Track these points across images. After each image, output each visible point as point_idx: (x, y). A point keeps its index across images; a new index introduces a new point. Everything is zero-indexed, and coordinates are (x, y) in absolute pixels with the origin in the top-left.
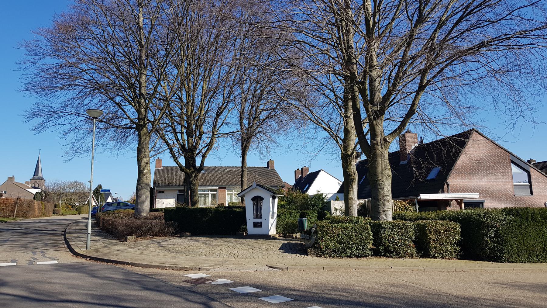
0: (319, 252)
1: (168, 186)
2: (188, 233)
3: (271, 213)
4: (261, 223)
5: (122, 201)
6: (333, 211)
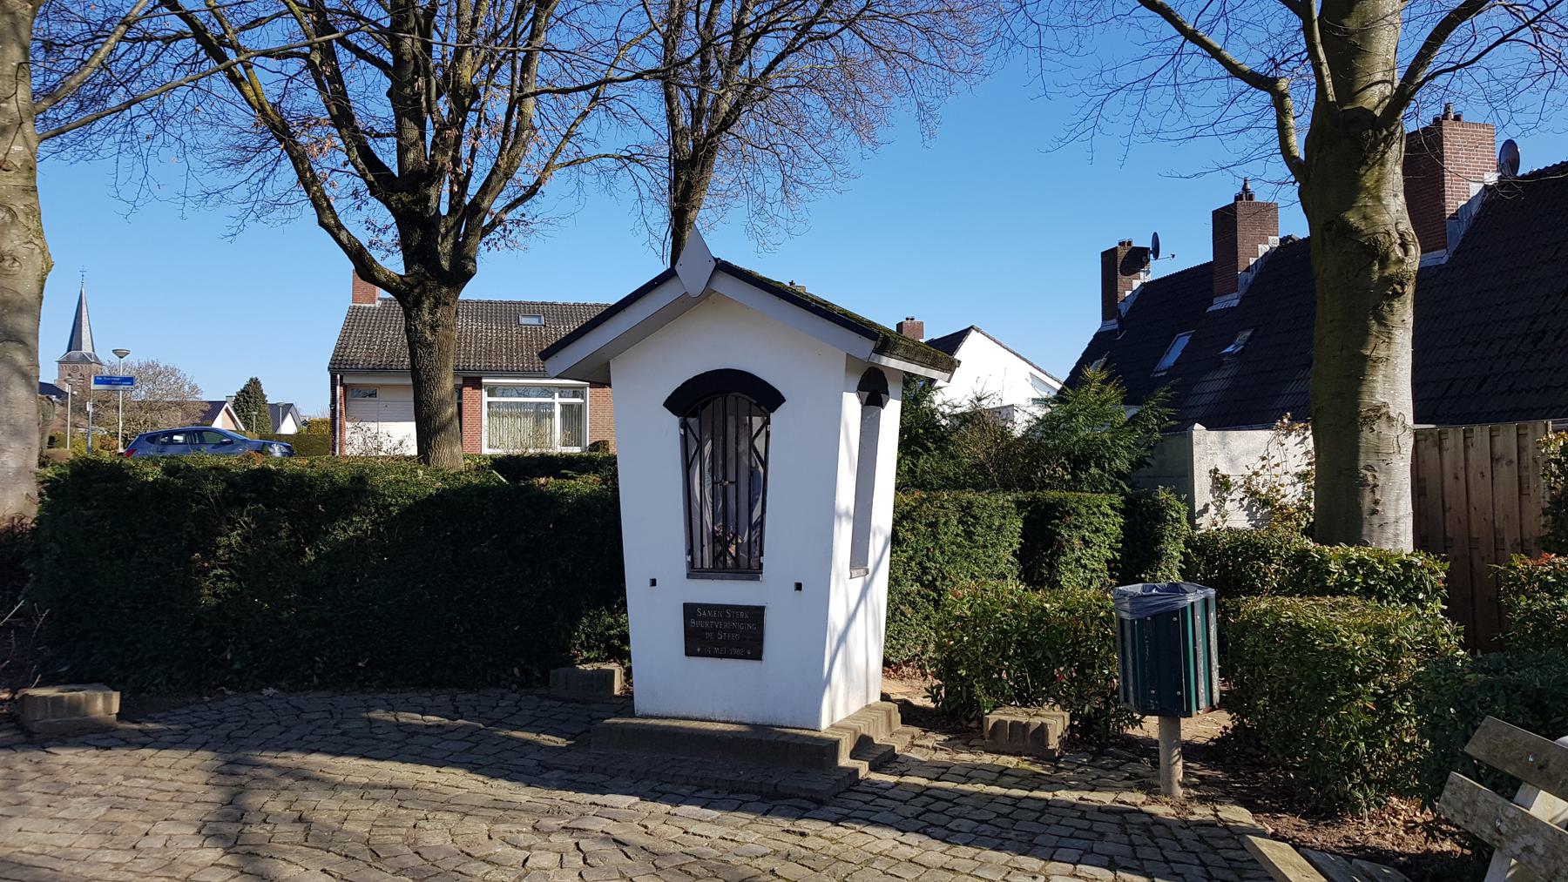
2: (104, 704)
3: (843, 535)
4: (756, 614)
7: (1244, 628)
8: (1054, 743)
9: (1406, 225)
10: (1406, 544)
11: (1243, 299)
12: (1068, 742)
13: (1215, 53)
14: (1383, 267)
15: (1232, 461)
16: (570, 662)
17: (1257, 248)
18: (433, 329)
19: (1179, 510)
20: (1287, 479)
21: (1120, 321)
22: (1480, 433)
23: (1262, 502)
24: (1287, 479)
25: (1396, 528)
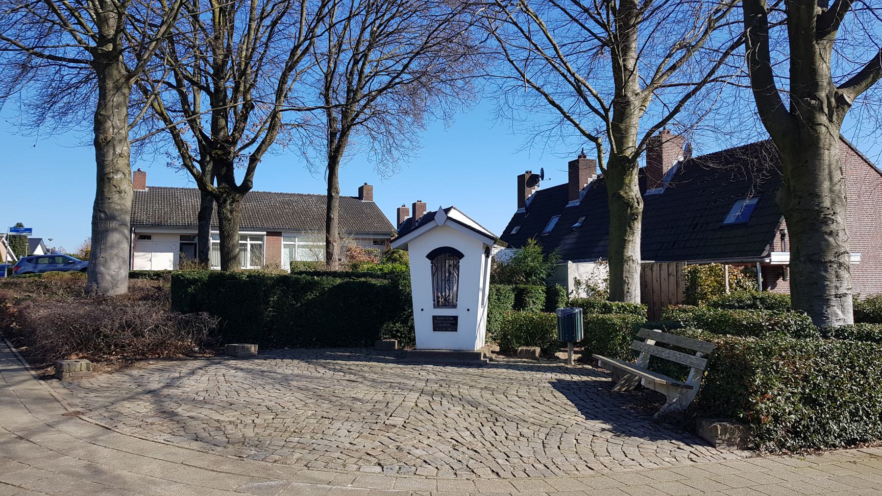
0: (753, 435)
1: (159, 225)
2: (254, 348)
4: (457, 317)
5: (62, 253)
6: (571, 286)
7: (589, 322)
8: (537, 355)
9: (639, 195)
10: (638, 300)
11: (581, 202)
12: (540, 356)
13: (576, 125)
14: (631, 210)
15: (580, 275)
16: (380, 339)
17: (589, 179)
18: (231, 212)
19: (563, 292)
20: (600, 281)
21: (526, 209)
22: (665, 265)
23: (591, 289)
24: (600, 281)
25: (635, 296)
